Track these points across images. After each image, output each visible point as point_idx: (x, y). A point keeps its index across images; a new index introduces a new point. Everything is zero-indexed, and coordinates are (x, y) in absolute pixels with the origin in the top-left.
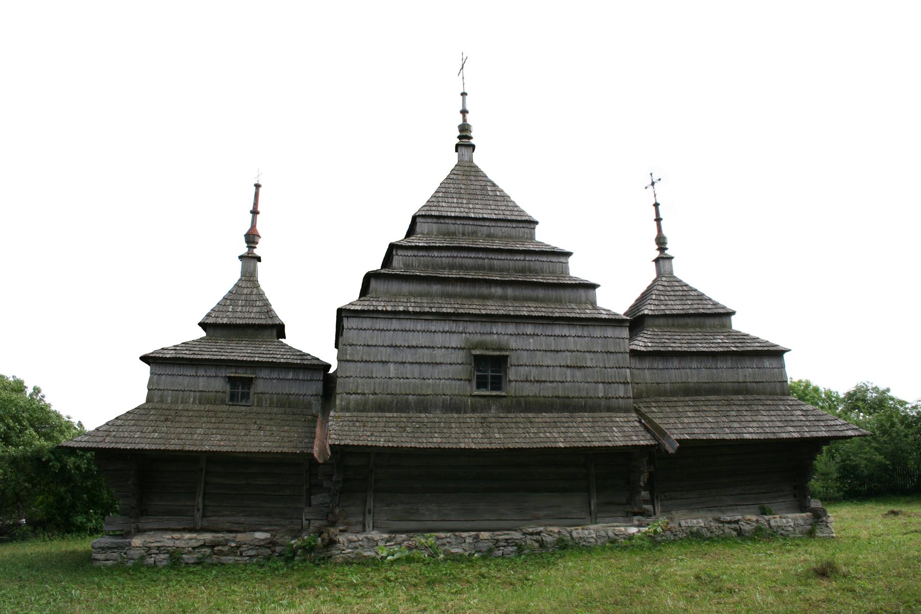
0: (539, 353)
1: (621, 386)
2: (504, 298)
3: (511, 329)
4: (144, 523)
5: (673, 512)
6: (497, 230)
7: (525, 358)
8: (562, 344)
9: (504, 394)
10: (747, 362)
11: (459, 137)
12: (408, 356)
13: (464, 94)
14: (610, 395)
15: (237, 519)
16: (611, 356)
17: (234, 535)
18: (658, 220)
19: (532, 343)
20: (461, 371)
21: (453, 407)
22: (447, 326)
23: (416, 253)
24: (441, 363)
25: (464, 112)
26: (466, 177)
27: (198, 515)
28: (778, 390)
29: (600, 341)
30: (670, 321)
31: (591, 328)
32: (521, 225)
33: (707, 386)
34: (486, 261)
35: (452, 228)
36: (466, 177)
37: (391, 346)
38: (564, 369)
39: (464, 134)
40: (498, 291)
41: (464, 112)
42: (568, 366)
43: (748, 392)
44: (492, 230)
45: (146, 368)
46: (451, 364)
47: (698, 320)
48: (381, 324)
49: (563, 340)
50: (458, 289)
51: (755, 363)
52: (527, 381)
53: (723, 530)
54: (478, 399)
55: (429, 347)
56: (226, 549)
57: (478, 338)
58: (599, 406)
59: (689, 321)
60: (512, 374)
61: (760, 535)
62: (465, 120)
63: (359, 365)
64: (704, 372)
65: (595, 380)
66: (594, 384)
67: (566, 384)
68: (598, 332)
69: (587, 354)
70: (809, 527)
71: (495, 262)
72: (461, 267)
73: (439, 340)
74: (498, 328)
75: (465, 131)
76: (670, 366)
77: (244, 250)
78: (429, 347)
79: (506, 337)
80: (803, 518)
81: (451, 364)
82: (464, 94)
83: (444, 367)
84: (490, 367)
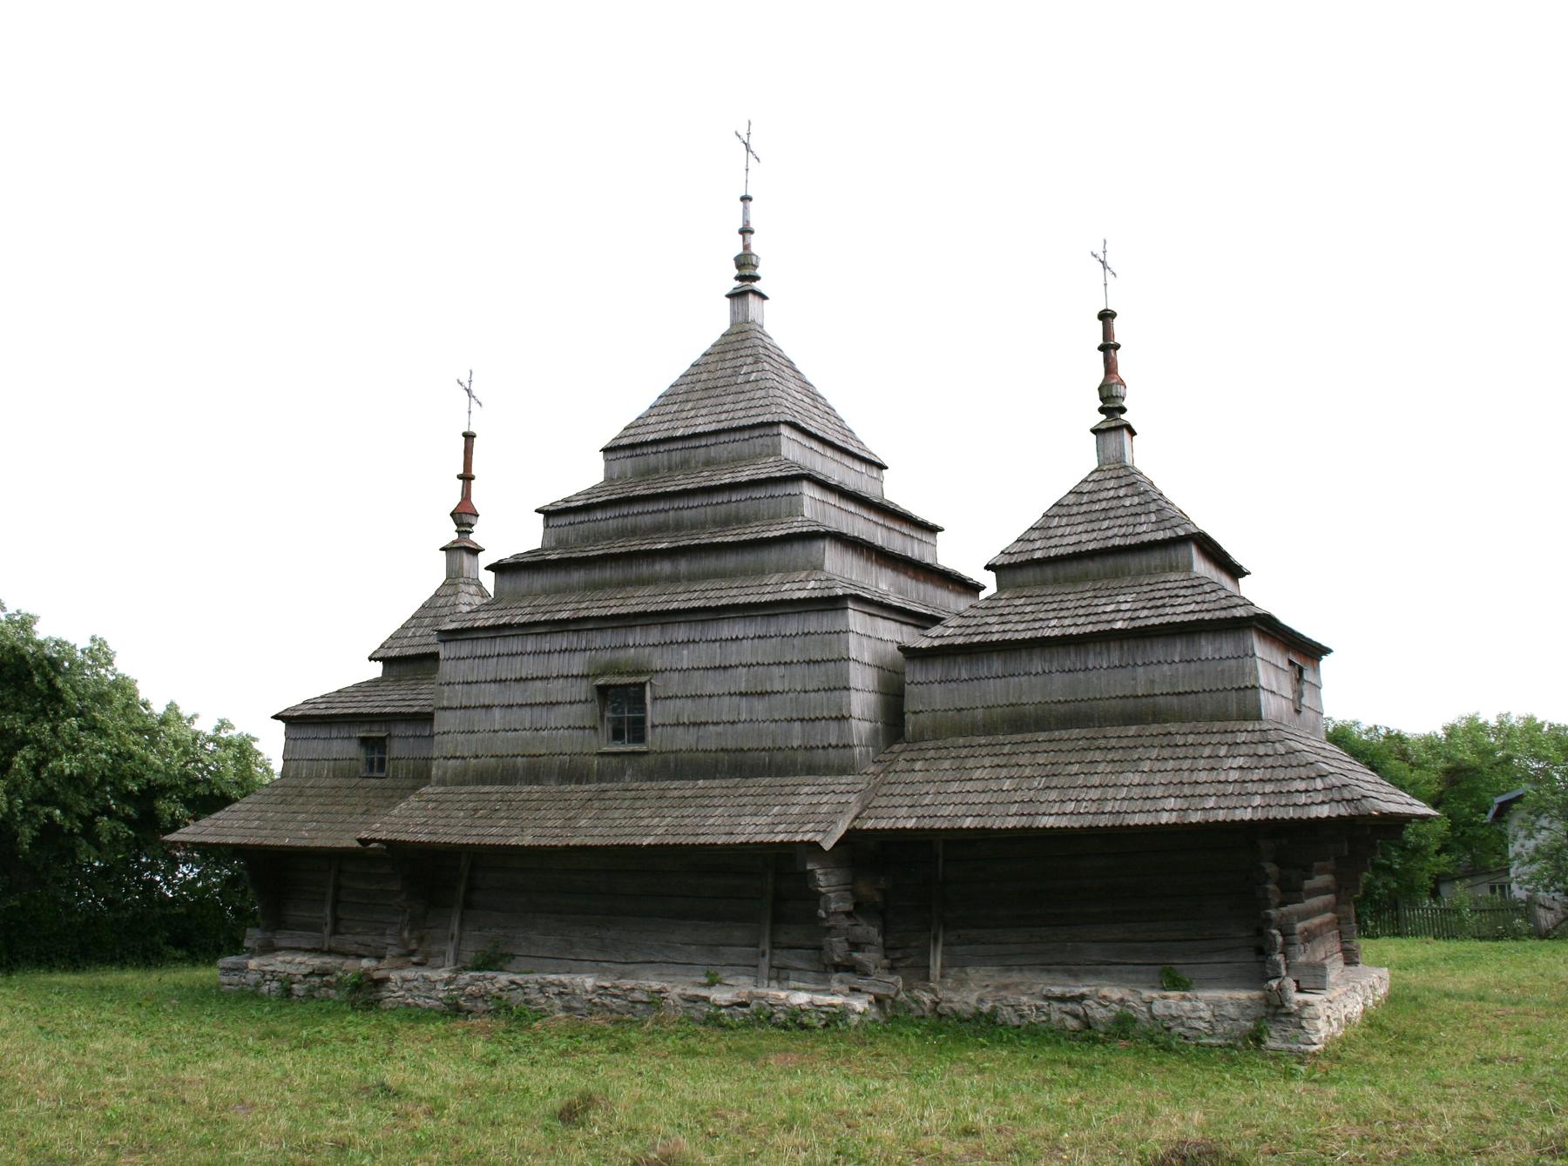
0: (697, 673)
1: (833, 725)
2: (674, 579)
3: (654, 635)
4: (282, 939)
5: (970, 970)
6: (723, 449)
7: (674, 683)
8: (733, 654)
9: (644, 748)
10: (1158, 651)
11: (739, 278)
12: (516, 694)
13: (746, 199)
14: (812, 743)
15: (368, 939)
16: (816, 669)
17: (339, 961)
18: (1108, 348)
19: (686, 657)
20: (583, 714)
21: (573, 774)
22: (562, 641)
23: (571, 518)
24: (558, 703)
25: (746, 231)
26: (740, 352)
27: (327, 930)
28: (1233, 708)
29: (796, 641)
30: (1049, 572)
31: (782, 619)
32: (756, 433)
33: (1062, 709)
34: (671, 513)
35: (652, 460)
36: (740, 352)
37: (495, 681)
38: (736, 699)
39: (747, 272)
40: (665, 567)
41: (746, 231)
42: (741, 694)
43: (1158, 717)
44: (713, 451)
45: (281, 725)
46: (571, 703)
47: (1110, 562)
48: (482, 648)
49: (734, 646)
50: (607, 573)
51: (1178, 650)
52: (678, 724)
53: (1048, 1015)
54: (607, 760)
55: (542, 678)
56: (333, 979)
57: (607, 656)
58: (794, 763)
59: (1093, 566)
60: (653, 713)
61: (1163, 1042)
62: (746, 247)
63: (459, 713)
64: (1059, 680)
65: (787, 715)
66: (785, 724)
67: (740, 726)
68: (792, 625)
69: (775, 669)
70: (1250, 1025)
71: (685, 513)
72: (634, 532)
73: (557, 664)
74: (636, 636)
75: (746, 266)
76: (984, 672)
77: (450, 534)
78: (542, 678)
79: (647, 650)
80: (1237, 1003)
81: (571, 703)
82: (746, 199)
83: (561, 710)
84: (621, 701)
